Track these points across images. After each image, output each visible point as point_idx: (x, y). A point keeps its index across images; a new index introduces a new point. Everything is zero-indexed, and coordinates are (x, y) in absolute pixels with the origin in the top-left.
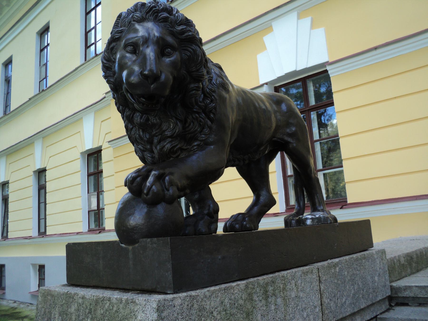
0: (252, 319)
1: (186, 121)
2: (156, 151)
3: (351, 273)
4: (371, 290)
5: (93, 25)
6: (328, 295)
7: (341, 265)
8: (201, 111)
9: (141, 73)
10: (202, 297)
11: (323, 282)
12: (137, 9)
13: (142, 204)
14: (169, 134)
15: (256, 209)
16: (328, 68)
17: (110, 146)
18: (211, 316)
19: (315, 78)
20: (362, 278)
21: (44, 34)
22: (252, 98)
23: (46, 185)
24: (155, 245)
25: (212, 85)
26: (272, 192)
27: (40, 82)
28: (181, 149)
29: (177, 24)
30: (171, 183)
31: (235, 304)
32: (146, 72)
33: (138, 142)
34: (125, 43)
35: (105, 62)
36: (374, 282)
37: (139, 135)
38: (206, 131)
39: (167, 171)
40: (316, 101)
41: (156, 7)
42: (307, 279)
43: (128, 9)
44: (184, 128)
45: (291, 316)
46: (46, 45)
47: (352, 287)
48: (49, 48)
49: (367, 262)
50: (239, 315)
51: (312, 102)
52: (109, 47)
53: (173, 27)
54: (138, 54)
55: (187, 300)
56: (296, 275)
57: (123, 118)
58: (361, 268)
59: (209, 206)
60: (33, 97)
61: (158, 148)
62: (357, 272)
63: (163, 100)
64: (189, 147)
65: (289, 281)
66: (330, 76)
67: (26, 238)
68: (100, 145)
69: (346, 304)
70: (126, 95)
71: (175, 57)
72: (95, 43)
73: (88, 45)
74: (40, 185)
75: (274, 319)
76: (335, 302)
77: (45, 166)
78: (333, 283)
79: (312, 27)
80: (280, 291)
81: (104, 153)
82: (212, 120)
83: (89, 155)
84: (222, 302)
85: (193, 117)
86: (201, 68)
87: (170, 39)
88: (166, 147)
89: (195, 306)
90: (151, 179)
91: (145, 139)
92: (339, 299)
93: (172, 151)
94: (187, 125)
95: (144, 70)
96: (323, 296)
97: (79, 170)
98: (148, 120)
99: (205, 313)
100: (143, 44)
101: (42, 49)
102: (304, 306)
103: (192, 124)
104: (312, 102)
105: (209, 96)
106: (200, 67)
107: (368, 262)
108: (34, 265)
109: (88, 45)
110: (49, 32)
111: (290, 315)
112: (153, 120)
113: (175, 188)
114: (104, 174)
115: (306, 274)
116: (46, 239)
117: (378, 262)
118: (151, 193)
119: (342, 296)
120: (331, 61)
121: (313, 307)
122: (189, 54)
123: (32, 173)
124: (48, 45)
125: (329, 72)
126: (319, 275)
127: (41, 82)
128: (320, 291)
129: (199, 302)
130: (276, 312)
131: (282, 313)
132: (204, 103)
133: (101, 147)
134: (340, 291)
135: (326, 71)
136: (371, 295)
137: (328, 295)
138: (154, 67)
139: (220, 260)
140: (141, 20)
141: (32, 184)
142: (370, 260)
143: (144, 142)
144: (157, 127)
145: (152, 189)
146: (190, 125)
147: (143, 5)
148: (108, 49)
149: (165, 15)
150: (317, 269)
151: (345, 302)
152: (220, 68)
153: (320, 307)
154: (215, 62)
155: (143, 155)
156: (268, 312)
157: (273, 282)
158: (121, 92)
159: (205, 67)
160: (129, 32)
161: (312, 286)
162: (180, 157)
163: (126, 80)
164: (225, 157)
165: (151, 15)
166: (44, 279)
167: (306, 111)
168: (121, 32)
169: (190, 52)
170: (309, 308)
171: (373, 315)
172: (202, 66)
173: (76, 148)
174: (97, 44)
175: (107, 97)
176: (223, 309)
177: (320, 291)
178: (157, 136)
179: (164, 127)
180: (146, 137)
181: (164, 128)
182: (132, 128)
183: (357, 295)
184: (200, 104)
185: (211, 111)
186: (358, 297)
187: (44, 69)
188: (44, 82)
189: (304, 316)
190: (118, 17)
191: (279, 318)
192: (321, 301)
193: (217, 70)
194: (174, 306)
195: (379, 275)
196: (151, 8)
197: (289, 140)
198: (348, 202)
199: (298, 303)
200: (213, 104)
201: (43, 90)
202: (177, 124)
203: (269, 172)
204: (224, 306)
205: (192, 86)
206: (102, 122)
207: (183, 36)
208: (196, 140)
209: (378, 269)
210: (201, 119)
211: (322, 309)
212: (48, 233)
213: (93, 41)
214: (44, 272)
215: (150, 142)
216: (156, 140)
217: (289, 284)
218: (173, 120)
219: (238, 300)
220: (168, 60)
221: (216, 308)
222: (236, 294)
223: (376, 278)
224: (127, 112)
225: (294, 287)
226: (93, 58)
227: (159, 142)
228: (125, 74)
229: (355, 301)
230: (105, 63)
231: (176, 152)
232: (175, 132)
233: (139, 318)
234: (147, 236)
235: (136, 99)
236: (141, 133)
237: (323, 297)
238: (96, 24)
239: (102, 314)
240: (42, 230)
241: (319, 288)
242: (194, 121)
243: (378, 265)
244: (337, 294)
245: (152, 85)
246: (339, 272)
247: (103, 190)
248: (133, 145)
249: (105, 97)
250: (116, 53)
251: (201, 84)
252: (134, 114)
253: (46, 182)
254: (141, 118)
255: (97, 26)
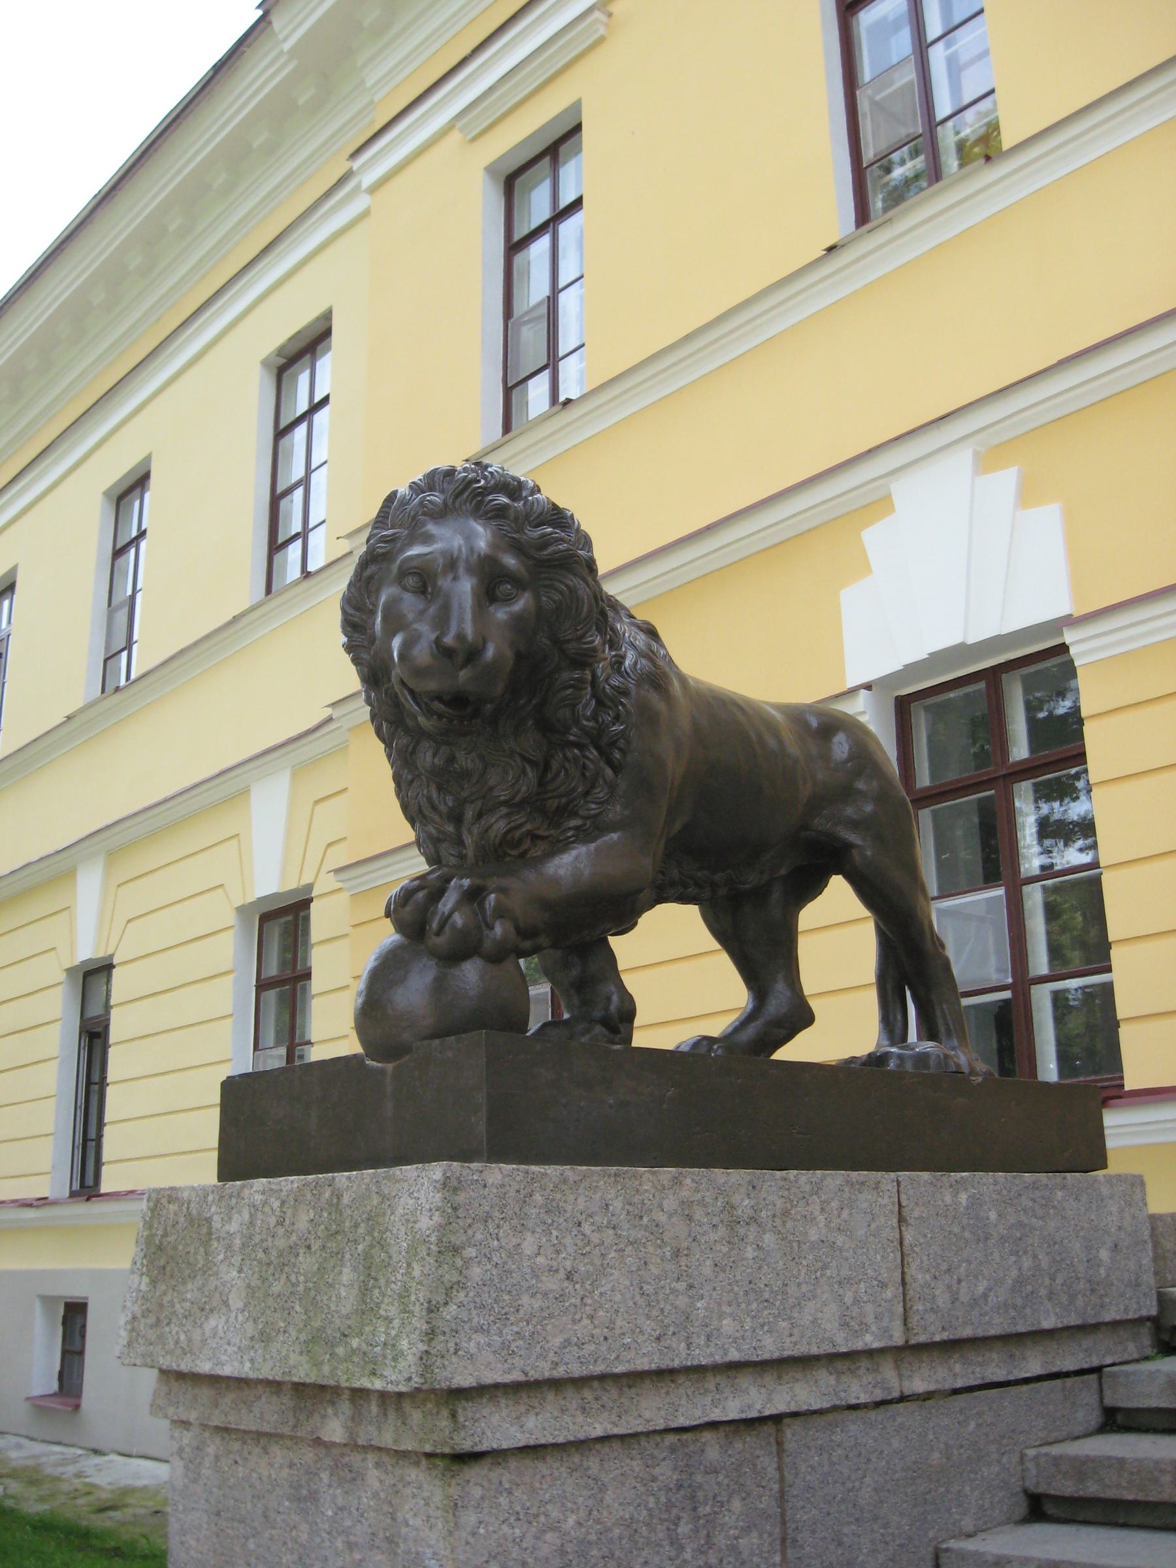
0: (687, 1266)
1: (547, 767)
2: (468, 840)
3: (1012, 1220)
4: (1082, 1285)
5: (298, 472)
6: (926, 1262)
7: (975, 1189)
8: (586, 741)
9: (438, 642)
10: (557, 1180)
11: (911, 1221)
12: (434, 485)
13: (425, 959)
14: (505, 795)
15: (750, 1032)
16: (1069, 637)
17: (340, 885)
18: (575, 1232)
19: (1032, 669)
20: (1051, 1243)
21: (133, 494)
22: (741, 718)
23: (109, 1019)
24: (450, 1054)
25: (622, 676)
26: (806, 992)
27: (106, 661)
28: (535, 837)
29: (530, 523)
30: (501, 912)
31: (641, 1217)
32: (449, 640)
33: (424, 816)
34: (400, 568)
35: (351, 611)
36: (1093, 1262)
37: (429, 799)
38: (600, 793)
39: (493, 883)
40: (1033, 748)
41: (479, 481)
42: (858, 1203)
43: (413, 483)
44: (541, 783)
45: (804, 1288)
46: (134, 533)
47: (1013, 1258)
48: (143, 544)
49: (1071, 1201)
50: (651, 1249)
51: (1020, 750)
52: (361, 575)
53: (520, 530)
54: (432, 594)
55: (518, 1179)
56: (825, 1183)
57: (389, 756)
58: (1048, 1213)
59: (609, 999)
60: (82, 710)
61: (476, 830)
62: (1034, 1220)
63: (489, 707)
64: (552, 832)
65: (801, 1195)
66: (1076, 664)
67: (27, 1204)
68: (306, 880)
69: (986, 1301)
70: (400, 695)
71: (522, 603)
72: (304, 535)
73: (281, 540)
74: (85, 1018)
75: (750, 1283)
76: (949, 1287)
77: (110, 952)
78: (946, 1234)
79: (1028, 495)
80: (774, 1216)
81: (316, 910)
82: (616, 769)
83: (265, 918)
84: (607, 1205)
85: (565, 756)
86: (590, 633)
87: (510, 561)
88: (495, 827)
89: (538, 1197)
90: (449, 901)
91: (443, 808)
92: (963, 1284)
93: (507, 841)
94: (549, 776)
95: (443, 634)
96: (911, 1260)
97: (229, 966)
98: (451, 759)
99: (561, 1220)
100: (445, 573)
101: (118, 546)
102: (845, 1272)
103: (563, 773)
104: (1020, 750)
105: (609, 703)
106: (585, 629)
107: (1077, 1199)
108: (48, 1301)
109: (281, 540)
110: (148, 490)
111: (799, 1285)
112: (465, 761)
113: (510, 926)
114: (317, 984)
115: (859, 1189)
116: (96, 1208)
117: (1114, 1209)
118: (447, 929)
119: (976, 1277)
120: (1077, 613)
121: (875, 1283)
122: (557, 597)
123: (62, 977)
124: (142, 534)
125: (1072, 651)
126: (899, 1201)
127: (109, 662)
128: (901, 1244)
129: (548, 1191)
130: (760, 1268)
131: (778, 1274)
132: (597, 721)
133: (310, 887)
134: (970, 1263)
135: (1063, 648)
136: (1080, 1296)
137: (927, 1263)
138: (469, 630)
139: (611, 1107)
140: (440, 514)
141: (59, 1015)
142: (1084, 1198)
143: (441, 817)
144: (474, 780)
145: (450, 921)
146: (558, 774)
147: (450, 473)
148: (360, 580)
149: (504, 500)
150: (895, 1184)
151: (985, 1296)
152: (651, 632)
153: (897, 1289)
154: (641, 615)
155: (437, 852)
156: (733, 1262)
157: (754, 1187)
158: (386, 686)
159: (599, 630)
160: (412, 540)
161: (873, 1226)
162: (528, 856)
163: (402, 656)
164: (647, 865)
165: (465, 502)
166: (81, 1353)
167: (995, 779)
168: (392, 540)
169: (561, 593)
170: (862, 1283)
171: (1088, 1360)
172: (590, 628)
173: (220, 891)
174: (311, 535)
175: (339, 718)
176: (609, 1223)
177: (901, 1244)
178: (472, 802)
179: (493, 779)
180: (445, 803)
181: (492, 783)
182: (412, 781)
183: (1029, 1288)
184: (585, 723)
185: (613, 744)
186: (1032, 1293)
187: (122, 617)
188: (120, 661)
189: (846, 1299)
190: (386, 500)
191: (766, 1285)
192: (903, 1273)
193: (641, 640)
194: (485, 1186)
195: (1116, 1246)
196: (468, 483)
197: (853, 838)
198: (1127, 1088)
199: (829, 1260)
200: (621, 725)
201: (117, 689)
202: (524, 772)
203: (800, 929)
204: (613, 1215)
205: (566, 675)
206: (317, 802)
207: (545, 553)
208: (574, 814)
209: (1113, 1230)
210: (587, 762)
211: (904, 1295)
212: (104, 1189)
213: (296, 527)
214: (84, 1326)
215: (457, 818)
216: (469, 814)
217: (802, 1203)
218: (515, 761)
219: (651, 1211)
220: (501, 614)
221: (590, 1216)
222: (647, 1195)
223: (1104, 1254)
224: (399, 739)
225: (817, 1213)
226: (296, 583)
227: (479, 816)
228: (396, 643)
229: (1019, 1302)
230: (351, 615)
231: (520, 842)
232: (518, 791)
233: (401, 1211)
234: (434, 1035)
235: (424, 707)
236: (435, 795)
237: (908, 1264)
238: (309, 471)
239: (312, 1220)
240: (90, 1181)
241: (898, 1237)
242: (567, 765)
243: (1114, 1219)
244: (959, 1266)
245: (461, 669)
246: (967, 1208)
247: (307, 1038)
248: (413, 828)
249: (329, 720)
250: (378, 591)
251: (588, 672)
252: (418, 743)
253: (107, 1007)
254: (434, 755)
255: (314, 476)
